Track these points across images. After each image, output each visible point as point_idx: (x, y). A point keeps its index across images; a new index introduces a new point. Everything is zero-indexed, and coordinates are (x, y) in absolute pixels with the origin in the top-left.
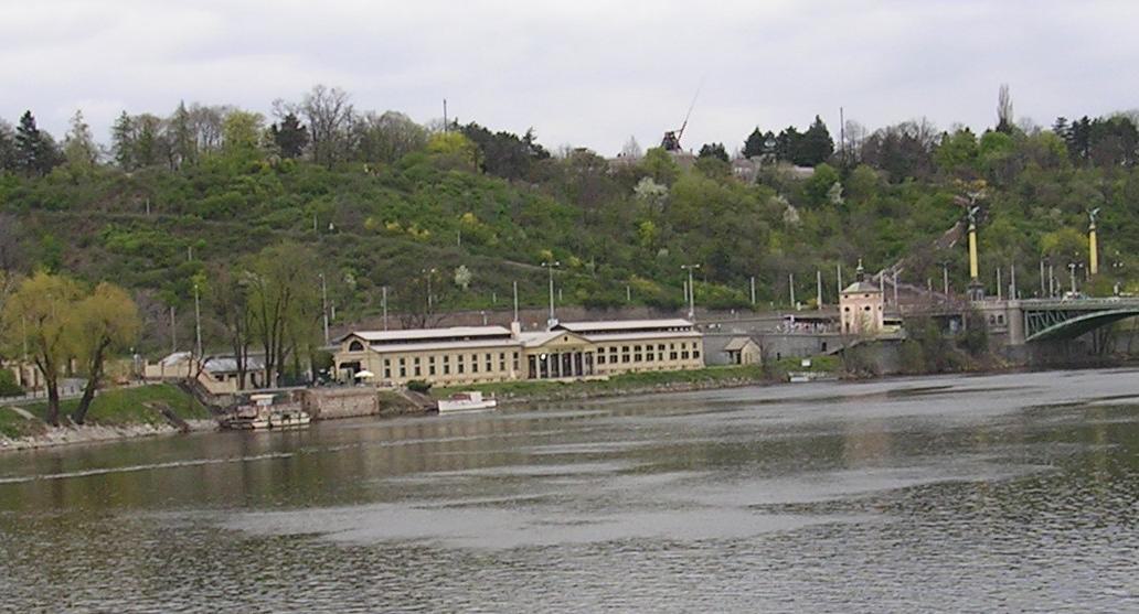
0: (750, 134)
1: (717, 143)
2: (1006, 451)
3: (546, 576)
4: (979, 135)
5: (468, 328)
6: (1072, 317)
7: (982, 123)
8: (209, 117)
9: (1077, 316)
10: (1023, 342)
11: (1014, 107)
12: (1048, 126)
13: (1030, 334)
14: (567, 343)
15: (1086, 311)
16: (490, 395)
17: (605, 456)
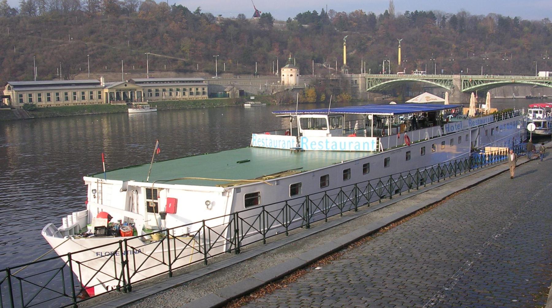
1: (268, 13)
2: (137, 151)
7: (378, 13)
8: (494, 14)
11: (395, 8)
12: (403, 13)
13: (368, 88)
15: (389, 80)
16: (155, 106)
17: (442, 174)
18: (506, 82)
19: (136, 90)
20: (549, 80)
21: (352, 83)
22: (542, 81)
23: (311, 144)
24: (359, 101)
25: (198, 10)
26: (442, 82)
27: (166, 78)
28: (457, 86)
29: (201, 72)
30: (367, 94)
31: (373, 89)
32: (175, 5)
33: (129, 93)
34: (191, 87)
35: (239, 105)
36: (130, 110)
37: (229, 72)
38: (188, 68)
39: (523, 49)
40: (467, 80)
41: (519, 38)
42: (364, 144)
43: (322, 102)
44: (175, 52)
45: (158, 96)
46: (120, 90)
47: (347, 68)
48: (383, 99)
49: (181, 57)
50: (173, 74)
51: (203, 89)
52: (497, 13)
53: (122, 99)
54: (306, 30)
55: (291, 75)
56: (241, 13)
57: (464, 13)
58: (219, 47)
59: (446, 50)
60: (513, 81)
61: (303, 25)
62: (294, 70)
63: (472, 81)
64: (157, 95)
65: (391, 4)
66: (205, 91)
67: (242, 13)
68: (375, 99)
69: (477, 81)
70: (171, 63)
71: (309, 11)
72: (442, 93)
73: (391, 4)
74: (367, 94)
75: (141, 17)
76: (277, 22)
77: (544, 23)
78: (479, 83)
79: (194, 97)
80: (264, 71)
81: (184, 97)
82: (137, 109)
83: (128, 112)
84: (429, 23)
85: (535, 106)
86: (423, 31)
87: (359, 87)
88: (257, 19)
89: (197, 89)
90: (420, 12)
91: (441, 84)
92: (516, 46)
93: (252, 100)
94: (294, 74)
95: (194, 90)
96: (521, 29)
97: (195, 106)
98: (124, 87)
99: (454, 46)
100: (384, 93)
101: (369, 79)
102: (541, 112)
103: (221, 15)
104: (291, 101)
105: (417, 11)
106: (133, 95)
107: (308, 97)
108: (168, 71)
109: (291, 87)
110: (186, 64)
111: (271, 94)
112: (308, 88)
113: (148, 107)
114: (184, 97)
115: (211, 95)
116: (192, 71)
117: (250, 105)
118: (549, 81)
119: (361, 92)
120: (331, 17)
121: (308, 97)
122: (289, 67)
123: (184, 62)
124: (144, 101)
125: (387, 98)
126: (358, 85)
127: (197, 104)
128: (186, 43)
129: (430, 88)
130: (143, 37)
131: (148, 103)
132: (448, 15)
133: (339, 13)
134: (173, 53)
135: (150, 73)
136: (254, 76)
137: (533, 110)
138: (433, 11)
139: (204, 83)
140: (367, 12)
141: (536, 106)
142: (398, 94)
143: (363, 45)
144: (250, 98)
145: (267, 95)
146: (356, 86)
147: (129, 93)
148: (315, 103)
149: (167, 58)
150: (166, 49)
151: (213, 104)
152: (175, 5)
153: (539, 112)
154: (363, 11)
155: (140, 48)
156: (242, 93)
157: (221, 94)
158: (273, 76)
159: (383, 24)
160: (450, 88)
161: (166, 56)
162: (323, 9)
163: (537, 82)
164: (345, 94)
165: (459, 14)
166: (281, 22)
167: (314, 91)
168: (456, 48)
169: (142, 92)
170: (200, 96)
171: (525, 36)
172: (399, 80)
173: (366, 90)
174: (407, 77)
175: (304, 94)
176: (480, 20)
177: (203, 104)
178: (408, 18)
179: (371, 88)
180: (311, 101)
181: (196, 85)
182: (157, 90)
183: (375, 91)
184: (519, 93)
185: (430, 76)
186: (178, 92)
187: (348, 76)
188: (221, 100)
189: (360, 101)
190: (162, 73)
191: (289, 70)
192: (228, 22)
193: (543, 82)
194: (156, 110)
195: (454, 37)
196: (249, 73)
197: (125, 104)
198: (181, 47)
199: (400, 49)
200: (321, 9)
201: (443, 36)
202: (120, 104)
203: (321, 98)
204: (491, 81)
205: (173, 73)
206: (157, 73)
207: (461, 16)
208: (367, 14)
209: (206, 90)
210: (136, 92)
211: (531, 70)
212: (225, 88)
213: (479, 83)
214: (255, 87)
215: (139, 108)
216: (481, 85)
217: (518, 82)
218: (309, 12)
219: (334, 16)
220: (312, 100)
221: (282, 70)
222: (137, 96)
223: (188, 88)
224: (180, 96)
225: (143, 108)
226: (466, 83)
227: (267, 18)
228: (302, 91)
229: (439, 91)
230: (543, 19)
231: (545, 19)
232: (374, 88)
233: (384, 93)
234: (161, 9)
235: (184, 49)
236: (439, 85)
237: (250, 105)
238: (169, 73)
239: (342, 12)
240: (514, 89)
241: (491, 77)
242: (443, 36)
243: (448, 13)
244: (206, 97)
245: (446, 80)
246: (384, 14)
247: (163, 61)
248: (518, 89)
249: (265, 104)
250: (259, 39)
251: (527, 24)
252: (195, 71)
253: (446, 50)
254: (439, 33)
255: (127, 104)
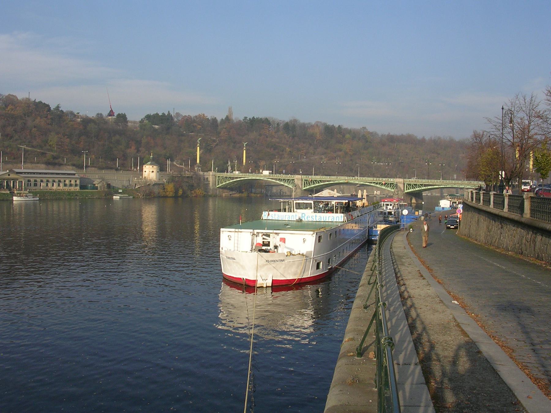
0: (13, 94)
1: (123, 113)
3: (171, 249)
4: (224, 119)
5: (28, 170)
6: (232, 179)
7: (220, 116)
8: (320, 122)
12: (241, 118)
13: (218, 185)
14: (9, 177)
15: (237, 178)
16: (37, 195)
18: (340, 182)
19: (17, 180)
20: (376, 181)
21: (204, 179)
22: (371, 181)
23: (307, 217)
24: (210, 196)
25: (58, 107)
26: (285, 181)
27: (36, 169)
28: (298, 184)
29: (69, 165)
30: (216, 190)
31: (222, 185)
32: (35, 100)
33: (12, 182)
34: (65, 179)
35: (108, 197)
36: (15, 198)
37: (93, 167)
38: (57, 161)
39: (346, 153)
40: (307, 180)
41: (342, 143)
42: (337, 217)
43: (179, 197)
44: (43, 145)
45: (36, 186)
46: (4, 179)
47: (200, 167)
48: (231, 195)
49: (49, 150)
50: (43, 166)
51: (76, 181)
52: (324, 120)
53: (5, 188)
54: (155, 130)
55: (153, 172)
56: (100, 112)
57: (295, 121)
58: (82, 143)
59: (281, 153)
60: (347, 181)
61: (153, 126)
62: (155, 167)
63: (312, 180)
64: (35, 185)
65: (230, 109)
66: (77, 183)
67: (101, 113)
68: (224, 195)
69: (316, 181)
70: (40, 155)
71: (157, 113)
72: (281, 190)
73: (230, 109)
74: (216, 190)
75: (9, 112)
76: (131, 122)
77: (362, 131)
78: (317, 183)
79: (67, 188)
80: (124, 167)
81: (59, 188)
82: (22, 197)
83: (13, 200)
84: (266, 129)
85: (385, 201)
86: (260, 135)
87: (209, 184)
88: (111, 118)
89: (70, 181)
90: (257, 118)
91: (284, 183)
92: (340, 150)
93: (120, 193)
94: (155, 171)
95: (67, 182)
96: (344, 136)
97: (70, 196)
98: (7, 176)
99: (288, 149)
100: (231, 189)
101: (218, 177)
102: (391, 205)
103: (79, 113)
104: (152, 195)
105: (254, 117)
106: (15, 185)
107: (167, 191)
108: (38, 163)
109: (152, 182)
110: (54, 158)
111: (135, 188)
112: (167, 183)
113: (31, 195)
114: (59, 188)
115: (82, 187)
116: (60, 165)
117: (119, 197)
118: (376, 182)
119: (211, 188)
120: (177, 119)
121: (167, 191)
122: (151, 164)
123: (53, 155)
124: (25, 191)
125: (234, 194)
126: (209, 182)
127: (71, 195)
128: (53, 139)
129: (270, 186)
130: (14, 130)
131: (29, 192)
132: (281, 122)
133: (185, 116)
134: (41, 147)
135: (25, 164)
136: (115, 172)
137: (385, 203)
138: (268, 118)
139: (76, 176)
140: (209, 115)
141: (387, 201)
142: (244, 191)
143: (209, 146)
144: (118, 191)
145: (131, 189)
146: (207, 183)
147: (12, 182)
148: (173, 197)
149: (36, 151)
150: (35, 143)
151: (85, 195)
152: (35, 100)
153: (389, 205)
154: (205, 115)
155: (11, 140)
156: (109, 186)
157: (91, 186)
158: (133, 172)
159: (225, 127)
160: (292, 186)
161: (35, 150)
162: (169, 111)
163: (366, 182)
164: (199, 189)
165: (291, 121)
166: (135, 122)
167: (173, 186)
168: (290, 151)
169: (23, 182)
170: (73, 188)
171: (347, 142)
172: (247, 178)
173: (216, 186)
174: (258, 176)
175: (164, 189)
176: (308, 127)
177: (76, 195)
178: (246, 123)
179: (221, 185)
180: (170, 195)
181: (70, 178)
182: (35, 181)
183: (224, 188)
184: (345, 191)
185: (278, 176)
186: (54, 183)
187: (201, 174)
188: (92, 192)
189: (211, 196)
190: (33, 165)
191: (151, 166)
192: (87, 121)
193: (371, 183)
194: (38, 199)
195: (288, 141)
196: (111, 168)
197: (9, 192)
198: (49, 141)
199: (245, 151)
200: (168, 111)
201: (277, 140)
202: (4, 192)
203: (178, 193)
204: (328, 181)
205: (42, 165)
206: (29, 165)
207: (293, 123)
208: (209, 118)
209: (78, 182)
210: (17, 182)
211: (354, 172)
212: (94, 181)
213: (317, 183)
214: (120, 181)
215: (22, 196)
216: (320, 184)
217: (351, 182)
218: (157, 114)
219: (180, 118)
220: (171, 194)
221: (144, 167)
222: (19, 186)
223: (62, 180)
224: (55, 187)
225: (26, 196)
226: (307, 182)
227: (122, 118)
228: (162, 186)
229: (278, 189)
230: (362, 127)
231: (363, 128)
232: (223, 185)
233: (231, 189)
234: (27, 105)
235: (51, 143)
236: (282, 183)
237: (119, 197)
238: (39, 165)
239: (187, 115)
240: (340, 188)
241: (328, 178)
242: (277, 140)
243: (281, 120)
244: (78, 188)
245: (289, 179)
246: (225, 118)
247: (34, 153)
248: (344, 188)
249: (132, 197)
250: (118, 137)
251: (349, 131)
252: (63, 165)
253: (281, 153)
254: (274, 137)
255: (10, 192)
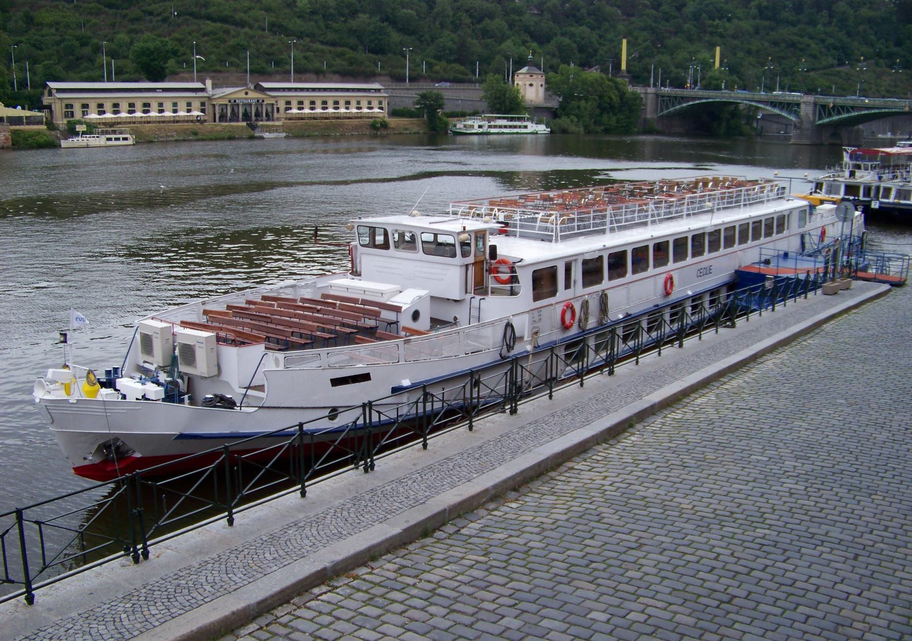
9: (862, 110)
10: (655, 117)
15: (694, 99)
